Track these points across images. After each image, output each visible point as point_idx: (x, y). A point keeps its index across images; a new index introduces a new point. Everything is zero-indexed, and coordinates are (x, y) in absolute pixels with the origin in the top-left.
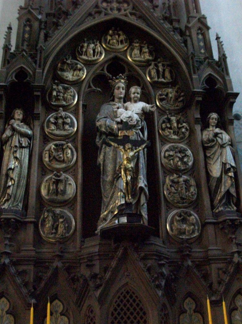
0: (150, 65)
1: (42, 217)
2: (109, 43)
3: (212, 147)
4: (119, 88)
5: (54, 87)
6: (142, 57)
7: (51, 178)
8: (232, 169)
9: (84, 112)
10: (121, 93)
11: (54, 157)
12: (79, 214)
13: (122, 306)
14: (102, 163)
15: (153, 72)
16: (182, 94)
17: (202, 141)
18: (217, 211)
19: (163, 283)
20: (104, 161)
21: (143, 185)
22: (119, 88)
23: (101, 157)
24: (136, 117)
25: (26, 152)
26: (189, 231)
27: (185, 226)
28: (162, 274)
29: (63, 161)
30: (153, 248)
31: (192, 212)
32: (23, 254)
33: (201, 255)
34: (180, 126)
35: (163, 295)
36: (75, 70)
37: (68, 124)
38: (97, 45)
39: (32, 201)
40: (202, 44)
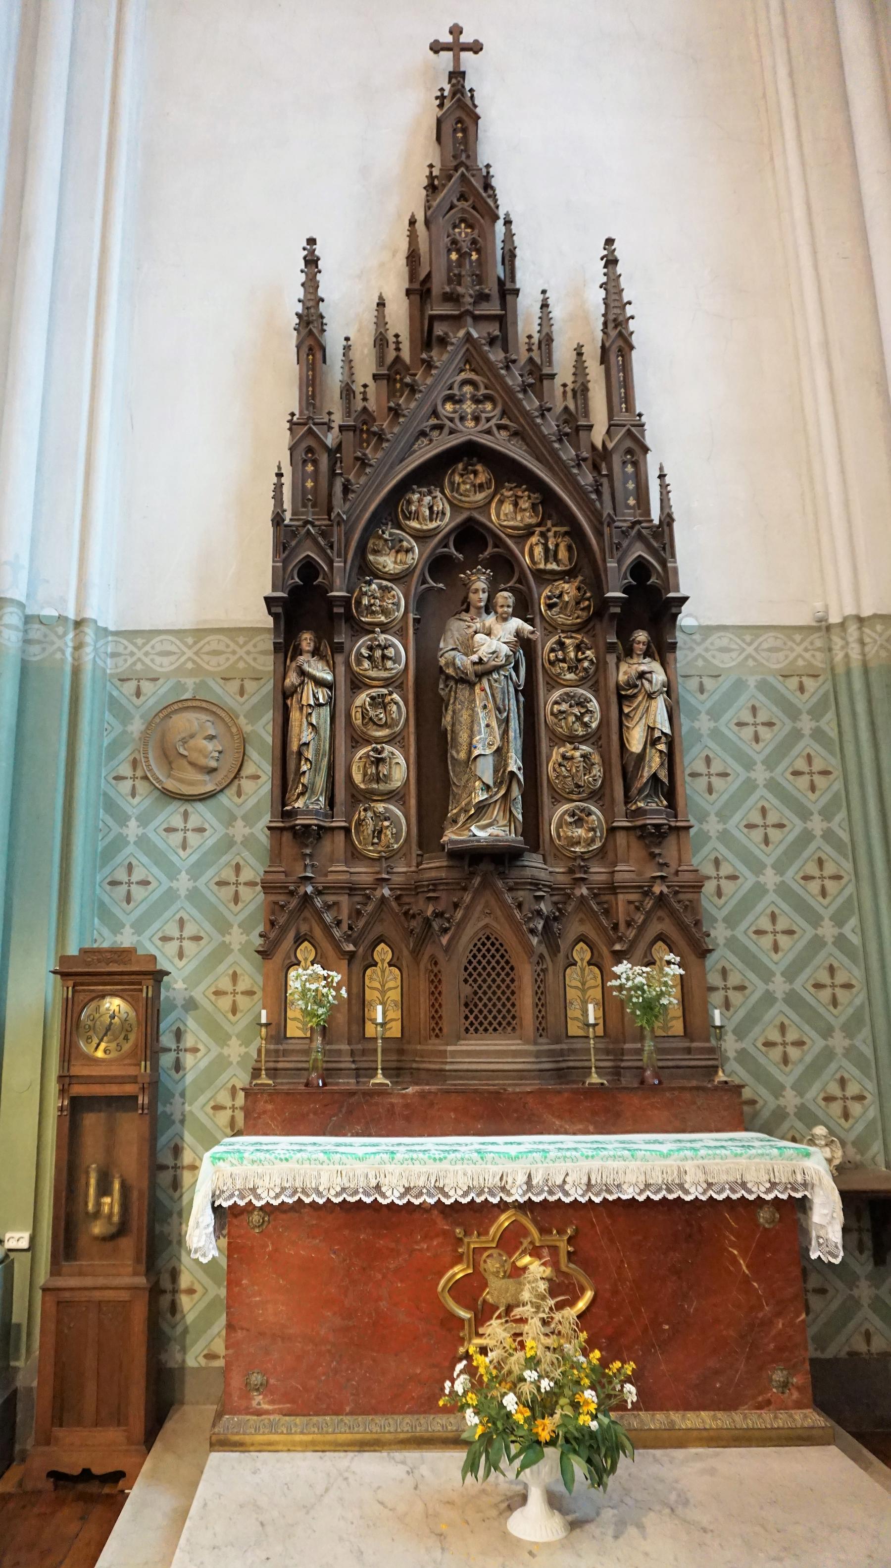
0: (533, 533)
1: (356, 817)
2: (458, 491)
3: (635, 696)
4: (476, 591)
5: (364, 589)
6: (519, 518)
7: (367, 755)
8: (663, 739)
9: (416, 631)
10: (480, 600)
11: (371, 719)
12: (413, 811)
13: (479, 957)
14: (449, 728)
15: (539, 551)
16: (588, 594)
17: (618, 687)
18: (634, 808)
19: (540, 927)
20: (453, 725)
21: (515, 770)
22: (476, 591)
23: (448, 718)
24: (505, 650)
25: (326, 712)
26: (585, 840)
27: (580, 831)
28: (539, 913)
29: (385, 725)
30: (528, 872)
31: (593, 808)
32: (331, 877)
33: (603, 878)
34: (580, 656)
35: (540, 942)
36: (397, 552)
37: (390, 659)
38: (436, 497)
39: (341, 795)
40: (631, 486)
